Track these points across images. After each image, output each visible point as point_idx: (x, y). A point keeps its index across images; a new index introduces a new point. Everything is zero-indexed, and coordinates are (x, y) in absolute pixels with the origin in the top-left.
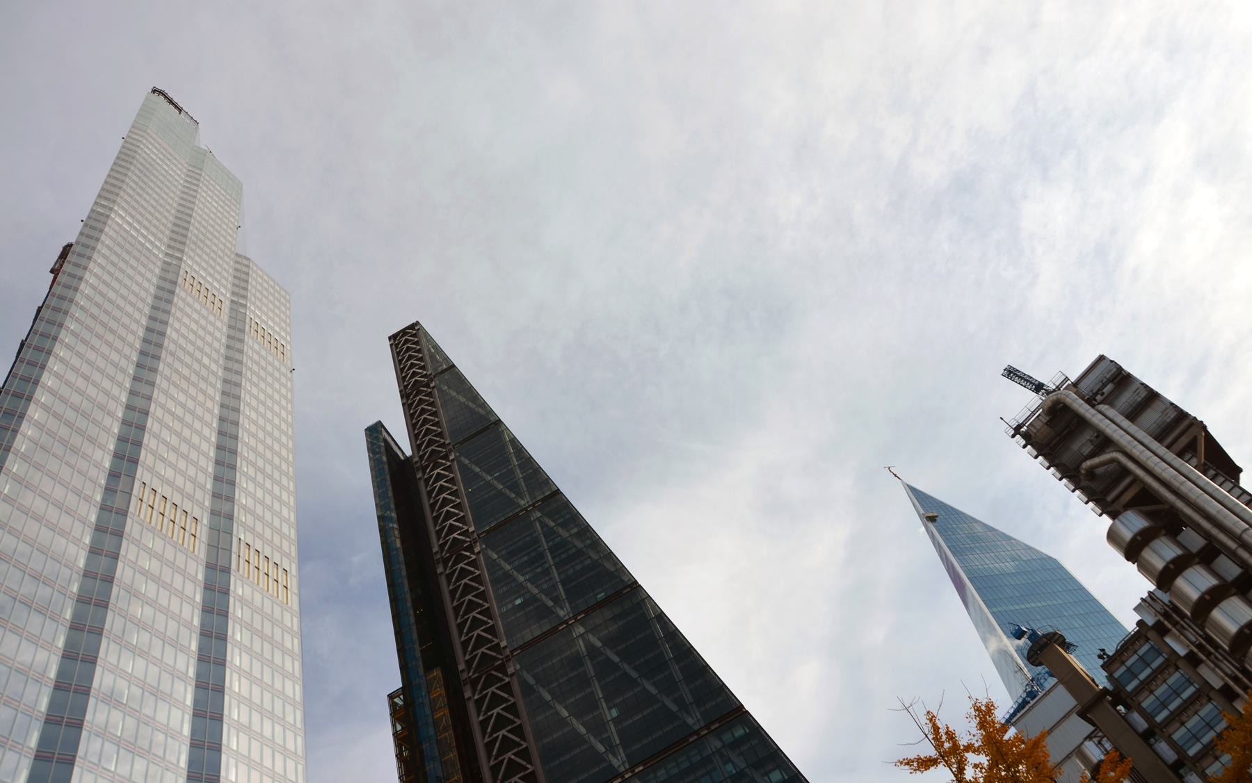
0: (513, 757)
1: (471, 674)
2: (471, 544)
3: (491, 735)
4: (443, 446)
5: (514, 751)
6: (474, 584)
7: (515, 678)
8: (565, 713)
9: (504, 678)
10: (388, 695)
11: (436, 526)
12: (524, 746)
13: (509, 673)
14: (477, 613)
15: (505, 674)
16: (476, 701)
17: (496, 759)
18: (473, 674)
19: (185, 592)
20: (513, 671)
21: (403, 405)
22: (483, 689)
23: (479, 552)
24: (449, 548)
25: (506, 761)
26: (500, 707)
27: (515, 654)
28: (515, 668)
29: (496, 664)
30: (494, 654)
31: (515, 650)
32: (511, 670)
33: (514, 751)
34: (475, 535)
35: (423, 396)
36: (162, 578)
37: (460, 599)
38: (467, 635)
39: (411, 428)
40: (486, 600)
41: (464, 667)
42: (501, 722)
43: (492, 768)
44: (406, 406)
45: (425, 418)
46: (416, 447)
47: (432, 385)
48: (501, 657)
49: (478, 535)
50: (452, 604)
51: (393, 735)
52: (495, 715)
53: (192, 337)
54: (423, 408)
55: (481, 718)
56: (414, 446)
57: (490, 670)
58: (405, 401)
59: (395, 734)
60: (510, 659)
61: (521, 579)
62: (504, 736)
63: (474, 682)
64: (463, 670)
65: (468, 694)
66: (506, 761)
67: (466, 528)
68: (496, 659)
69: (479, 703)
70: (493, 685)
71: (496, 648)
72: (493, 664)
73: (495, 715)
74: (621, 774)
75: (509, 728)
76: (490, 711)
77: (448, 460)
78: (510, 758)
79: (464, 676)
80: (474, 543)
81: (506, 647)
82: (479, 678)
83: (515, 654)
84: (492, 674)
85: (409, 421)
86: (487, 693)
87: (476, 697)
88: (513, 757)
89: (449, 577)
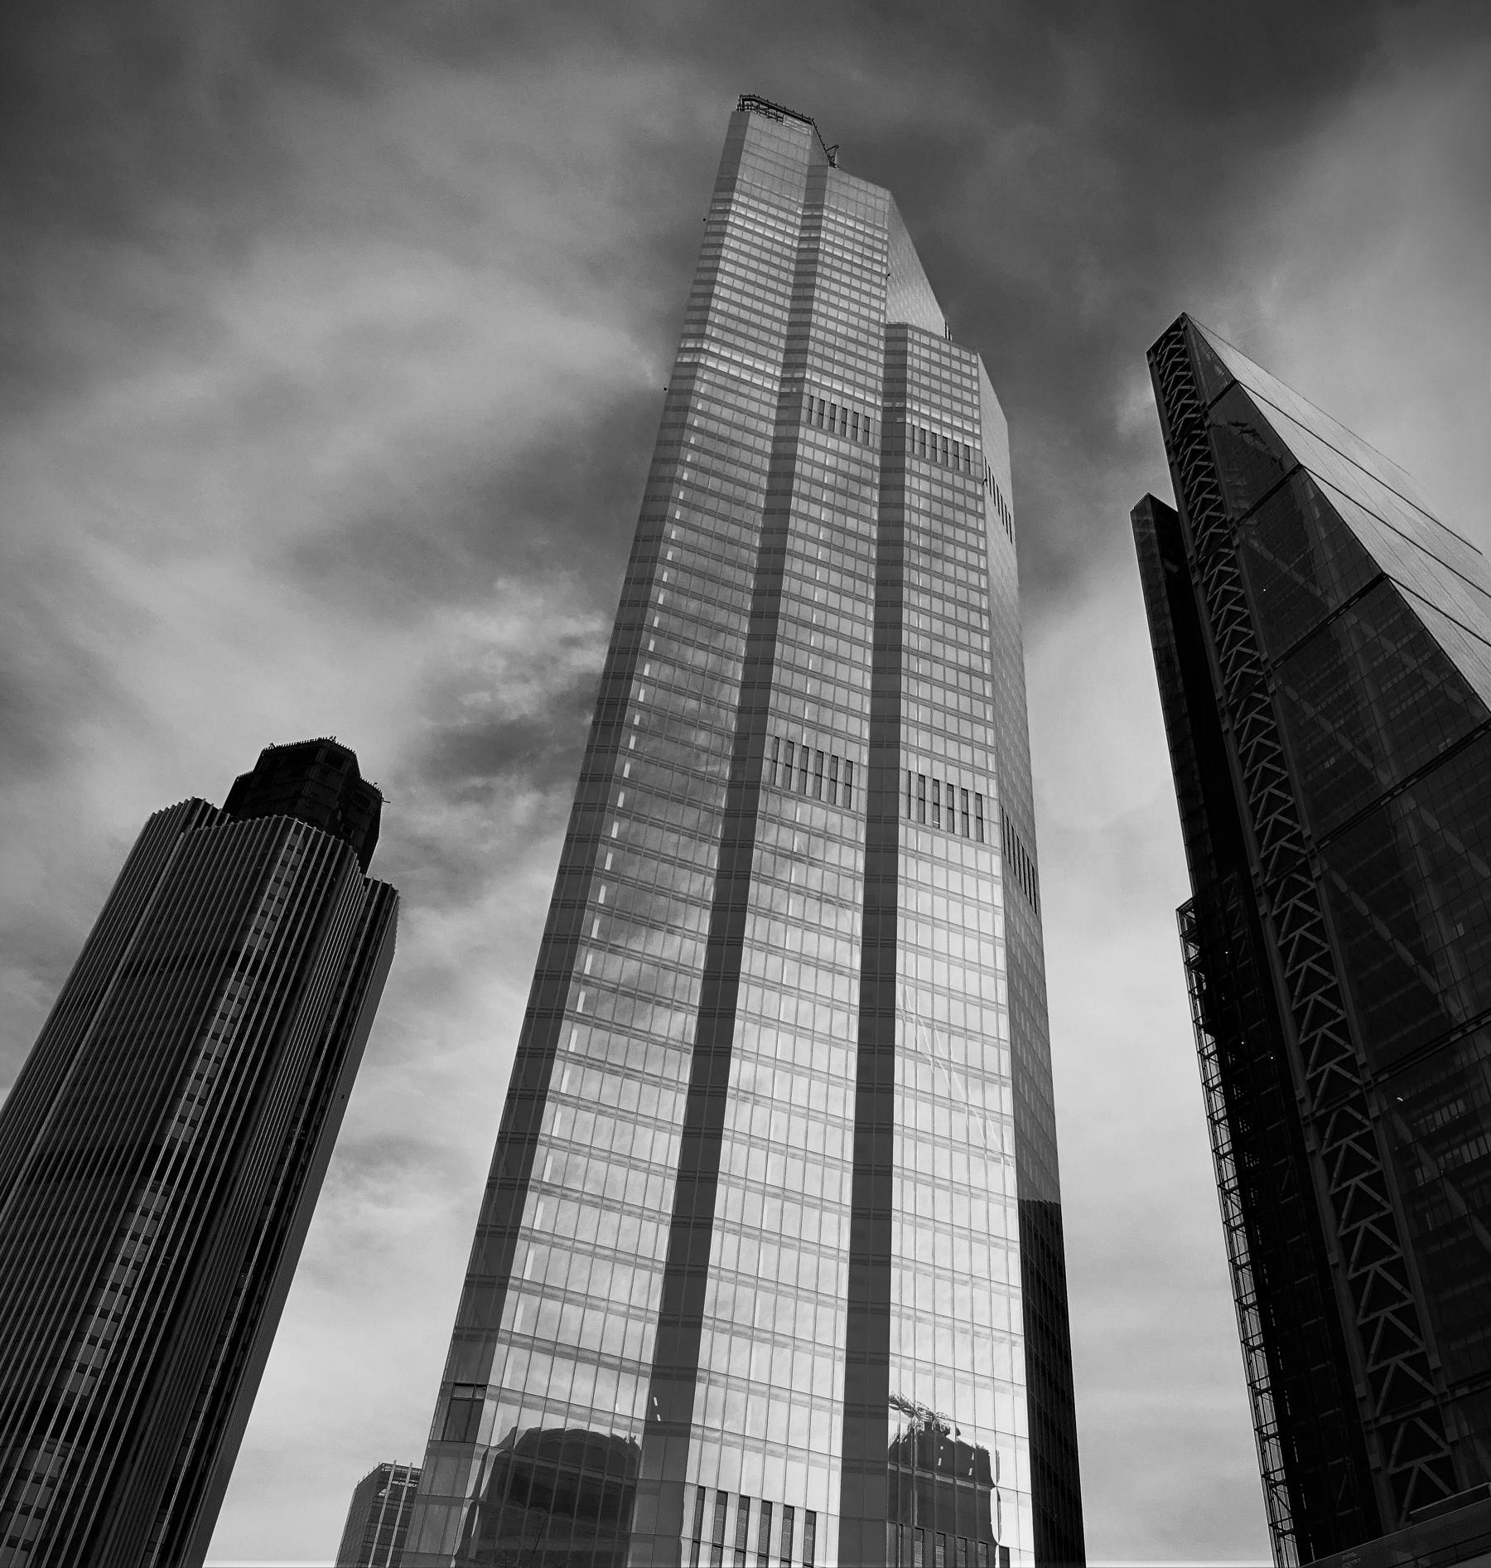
0: (1320, 998)
1: (1267, 879)
2: (1306, 863)
3: (1286, 936)
4: (1224, 525)
5: (1321, 990)
6: (1269, 743)
7: (1321, 883)
8: (1386, 934)
9: (1309, 883)
10: (1177, 910)
11: (1255, 823)
12: (1335, 983)
13: (1314, 877)
14: (1223, 565)
15: (1267, 694)
16: (1275, 918)
17: (1307, 1034)
18: (1318, 1109)
19: (975, 910)
20: (1378, 1113)
21: (1171, 465)
22: (1283, 901)
23: (1274, 693)
24: (1237, 691)
25: (1311, 1004)
26: (1303, 928)
27: (1322, 846)
28: (1380, 1109)
29: (1298, 864)
30: (1295, 848)
31: (1322, 840)
32: (1316, 873)
33: (1321, 990)
34: (1312, 845)
35: (1183, 385)
36: (961, 685)
37: (1247, 742)
38: (1300, 1001)
39: (1179, 483)
40: (1283, 767)
41: (1303, 1095)
42: (1306, 948)
43: (1333, 1197)
44: (1175, 466)
45: (1196, 465)
46: (1183, 496)
47: (1206, 424)
48: (1261, 673)
49: (1273, 666)
50: (1253, 827)
51: (1185, 963)
52: (1297, 938)
53: (946, 389)
54: (1221, 571)
55: (1281, 943)
56: (1180, 496)
57: (1290, 873)
58: (1172, 459)
59: (1189, 964)
60: (1371, 1089)
61: (1329, 728)
62: (1332, 1072)
63: (1233, 710)
64: (1257, 875)
65: (1310, 1146)
66: (1311, 1004)
67: (1257, 654)
68: (1298, 855)
69: (1330, 1160)
70: (1348, 1135)
71: (1297, 839)
72: (1348, 1096)
73: (1297, 938)
74: (1461, 1025)
75: (1315, 957)
76: (1306, 996)
77: (1231, 547)
78: (1316, 1001)
79: (1259, 883)
80: (1312, 858)
81: (1309, 837)
82: (1277, 885)
83: (1322, 846)
84: (1293, 878)
85: (1179, 491)
86: (1324, 1071)
87: (1275, 913)
88: (1320, 998)
89: (1238, 733)
